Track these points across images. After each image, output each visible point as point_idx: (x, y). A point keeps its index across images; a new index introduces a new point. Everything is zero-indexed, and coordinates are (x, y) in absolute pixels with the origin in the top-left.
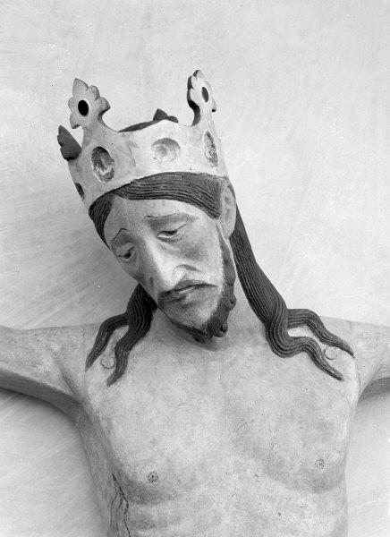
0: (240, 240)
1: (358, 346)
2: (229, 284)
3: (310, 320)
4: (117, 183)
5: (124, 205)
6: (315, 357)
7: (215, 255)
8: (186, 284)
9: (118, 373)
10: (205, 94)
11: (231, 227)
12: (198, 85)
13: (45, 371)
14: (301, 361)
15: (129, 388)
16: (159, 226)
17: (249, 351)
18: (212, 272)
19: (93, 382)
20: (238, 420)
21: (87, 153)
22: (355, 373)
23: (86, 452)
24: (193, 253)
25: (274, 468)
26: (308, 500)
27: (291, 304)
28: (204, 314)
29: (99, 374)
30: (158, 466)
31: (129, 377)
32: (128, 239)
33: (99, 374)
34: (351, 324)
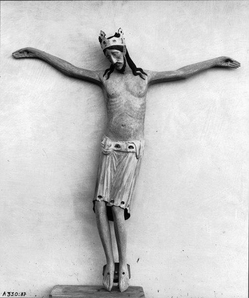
0: (127, 55)
1: (148, 74)
2: (125, 63)
3: (140, 70)
4: (107, 47)
5: (108, 50)
6: (141, 77)
7: (122, 58)
8: (117, 63)
9: (108, 78)
10: (121, 32)
11: (125, 53)
12: (120, 30)
13: (96, 77)
14: (138, 77)
15: (109, 81)
16: (113, 53)
17: (130, 75)
18: (122, 61)
19: (104, 79)
20: (127, 85)
21: (103, 42)
22: (147, 79)
23: (103, 92)
24: (118, 58)
25: (132, 93)
26: (138, 99)
27: (137, 67)
28: (121, 68)
29: (105, 78)
30: (114, 92)
31: (110, 78)
32: (108, 56)
33: (105, 78)
34: (148, 71)
